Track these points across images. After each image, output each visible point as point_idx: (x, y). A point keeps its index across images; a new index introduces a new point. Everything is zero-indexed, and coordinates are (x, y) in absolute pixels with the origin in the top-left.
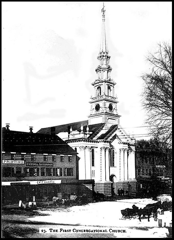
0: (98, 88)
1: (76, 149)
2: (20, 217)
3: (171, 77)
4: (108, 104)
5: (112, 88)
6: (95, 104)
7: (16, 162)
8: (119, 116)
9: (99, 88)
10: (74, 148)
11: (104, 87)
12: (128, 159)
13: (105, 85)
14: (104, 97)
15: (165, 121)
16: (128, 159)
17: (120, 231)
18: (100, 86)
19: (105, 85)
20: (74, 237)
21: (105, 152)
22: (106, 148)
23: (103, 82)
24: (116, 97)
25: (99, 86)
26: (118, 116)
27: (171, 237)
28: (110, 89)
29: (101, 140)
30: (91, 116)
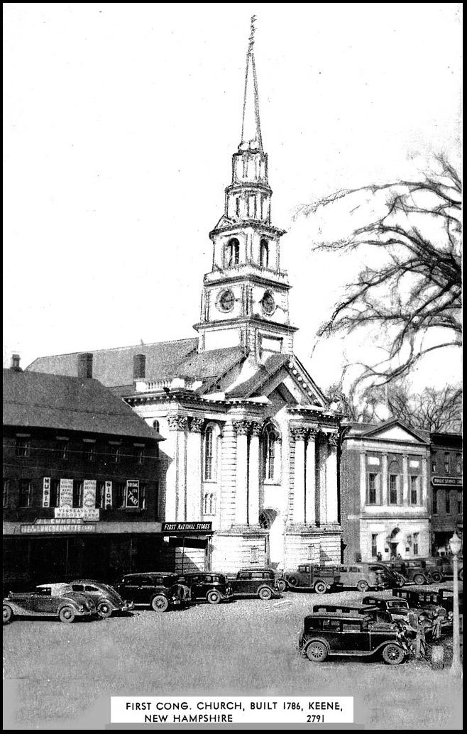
0: (230, 244)
1: (156, 424)
2: (30, 614)
3: (457, 189)
4: (259, 293)
5: (272, 244)
6: (219, 290)
7: (74, 528)
8: (292, 330)
9: (234, 243)
10: (150, 423)
11: (250, 240)
12: (355, 190)
13: (246, 226)
14: (248, 271)
15: (412, 350)
16: (307, 451)
17: (225, 706)
18: (235, 237)
19: (246, 226)
20: (6, 673)
21: (249, 443)
22: (252, 426)
23: (247, 224)
24: (285, 273)
25: (232, 237)
26: (289, 329)
27: (444, 592)
28: (267, 248)
29: (237, 400)
30: (207, 323)
